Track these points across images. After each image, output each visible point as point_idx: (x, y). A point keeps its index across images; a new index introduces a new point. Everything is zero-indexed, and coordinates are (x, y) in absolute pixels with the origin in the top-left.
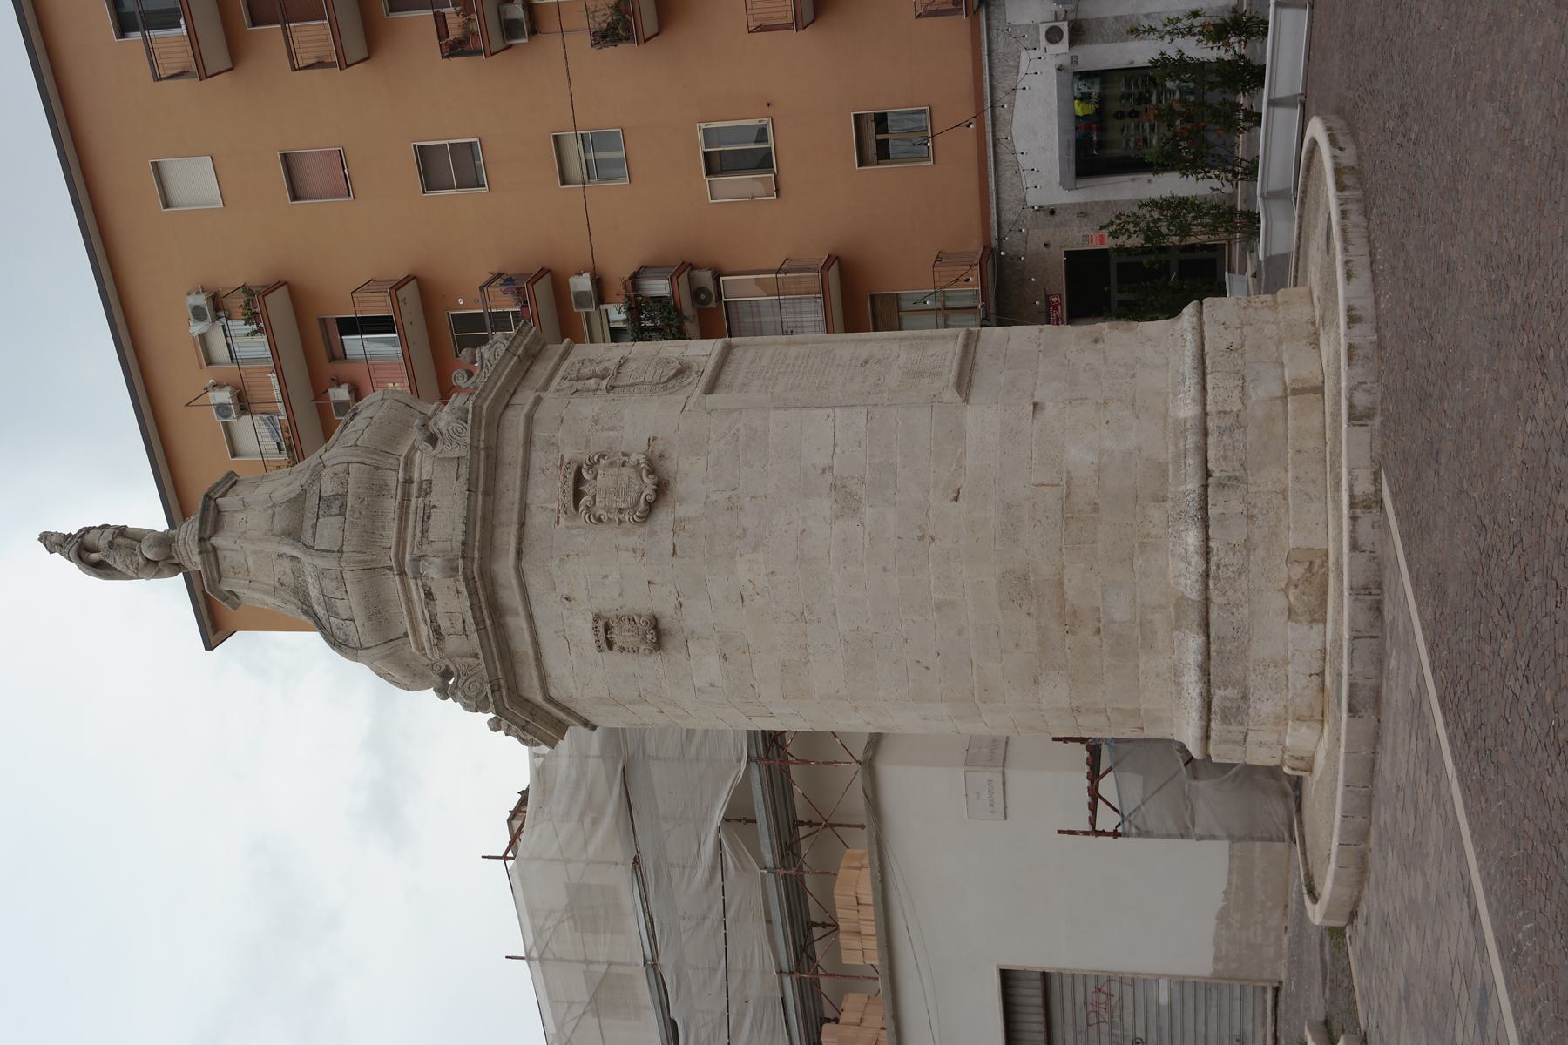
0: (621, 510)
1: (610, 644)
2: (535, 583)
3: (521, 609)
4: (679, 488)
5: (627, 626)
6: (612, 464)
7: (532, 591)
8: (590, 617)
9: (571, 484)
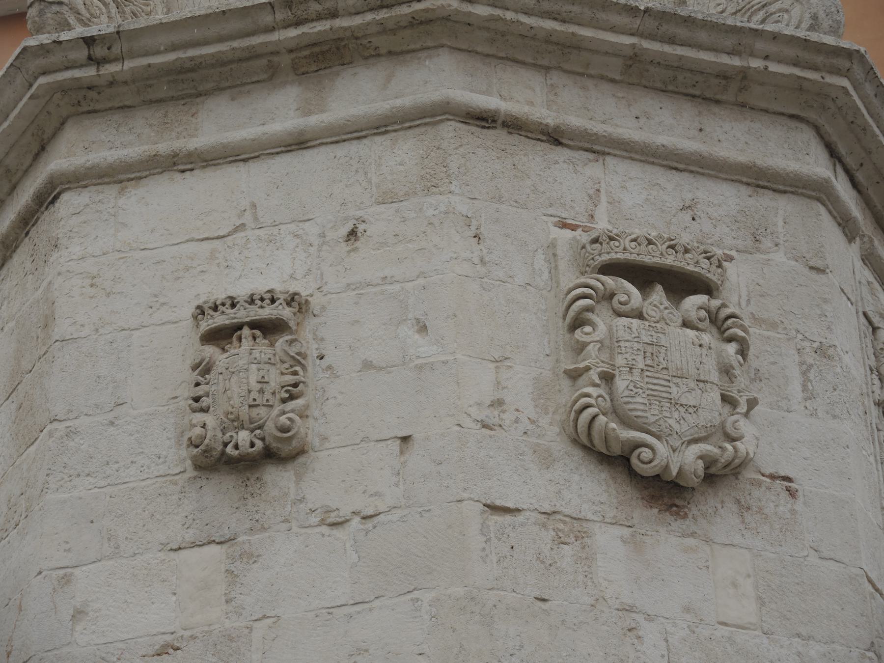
0: (608, 378)
1: (220, 336)
2: (399, 155)
3: (315, 120)
4: (667, 541)
5: (275, 379)
6: (726, 371)
7: (376, 146)
8: (302, 288)
9: (670, 260)
